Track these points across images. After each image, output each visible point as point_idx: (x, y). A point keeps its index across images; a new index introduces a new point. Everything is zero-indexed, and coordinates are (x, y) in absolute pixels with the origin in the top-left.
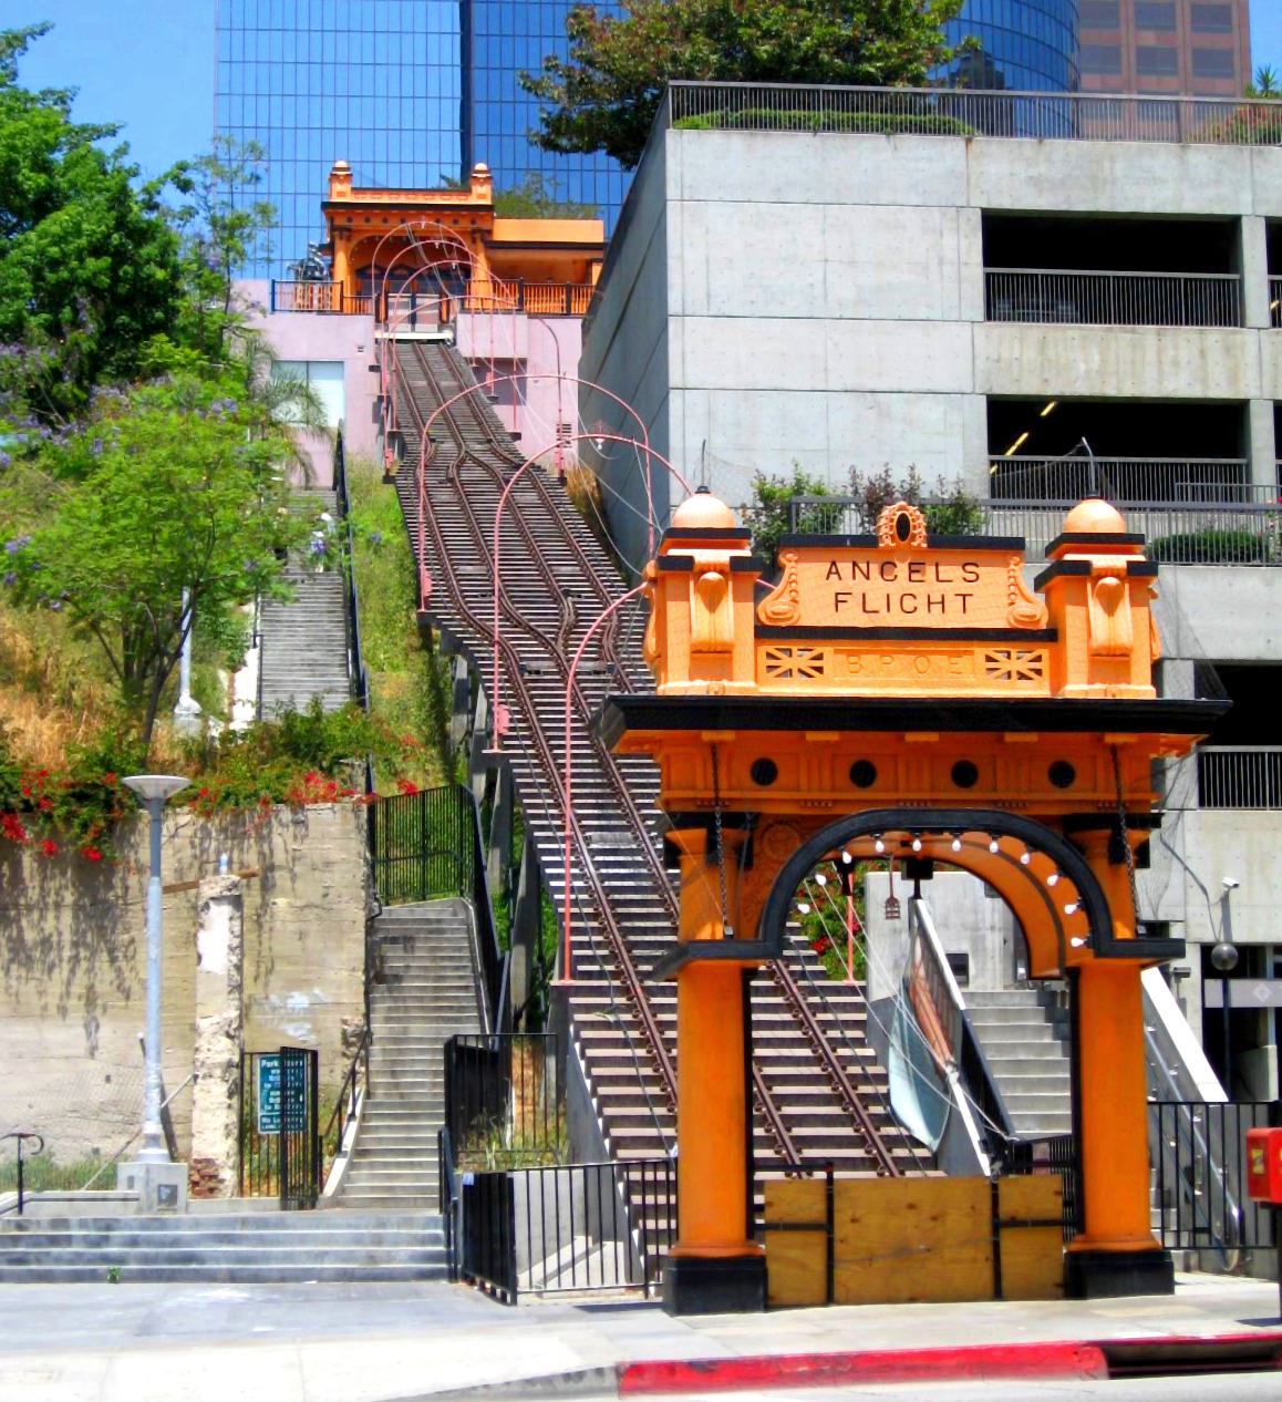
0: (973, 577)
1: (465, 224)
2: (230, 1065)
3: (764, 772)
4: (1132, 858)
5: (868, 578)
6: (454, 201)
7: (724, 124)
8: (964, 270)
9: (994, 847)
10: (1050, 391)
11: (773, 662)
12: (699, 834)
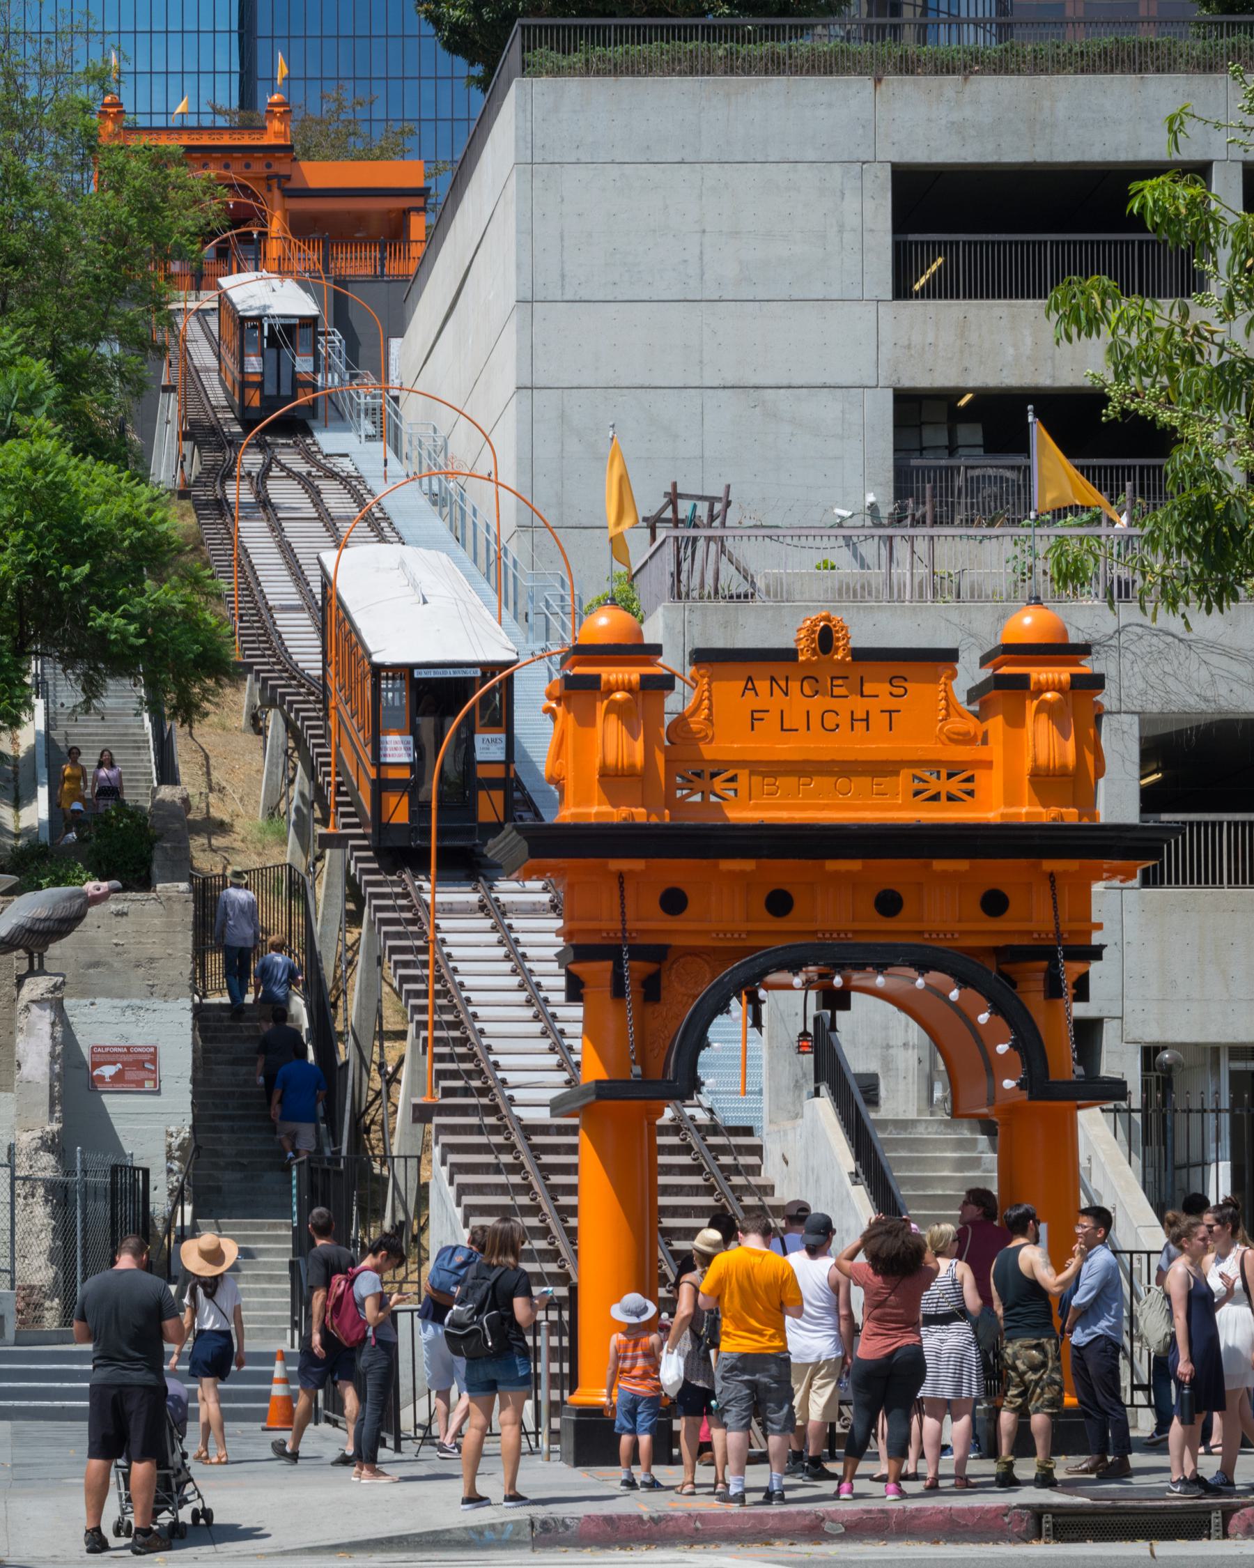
0: (902, 691)
1: (258, 168)
3: (674, 902)
4: (1069, 991)
6: (246, 141)
7: (587, 70)
9: (920, 982)
10: (971, 384)
12: (604, 968)
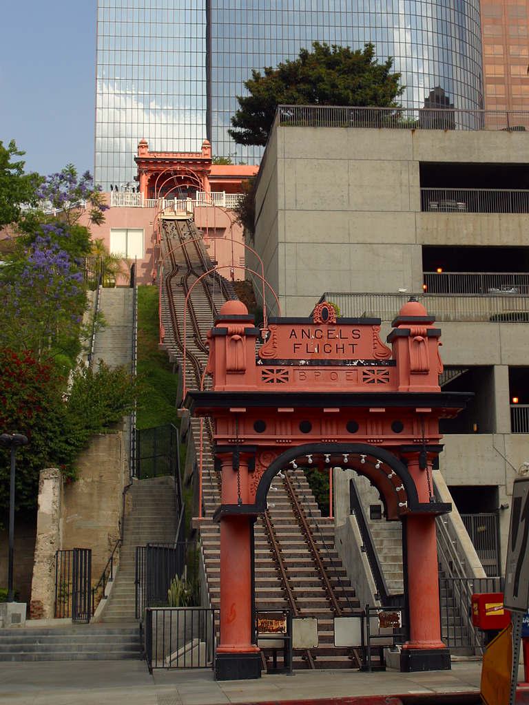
2: (51, 556)
8: (411, 189)
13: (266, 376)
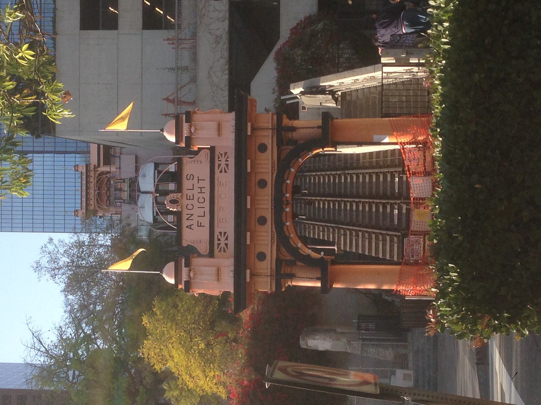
5: (192, 215)
11: (222, 249)
13: (222, 249)
